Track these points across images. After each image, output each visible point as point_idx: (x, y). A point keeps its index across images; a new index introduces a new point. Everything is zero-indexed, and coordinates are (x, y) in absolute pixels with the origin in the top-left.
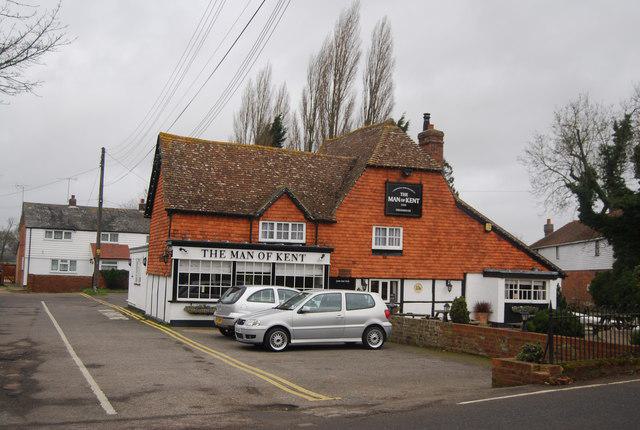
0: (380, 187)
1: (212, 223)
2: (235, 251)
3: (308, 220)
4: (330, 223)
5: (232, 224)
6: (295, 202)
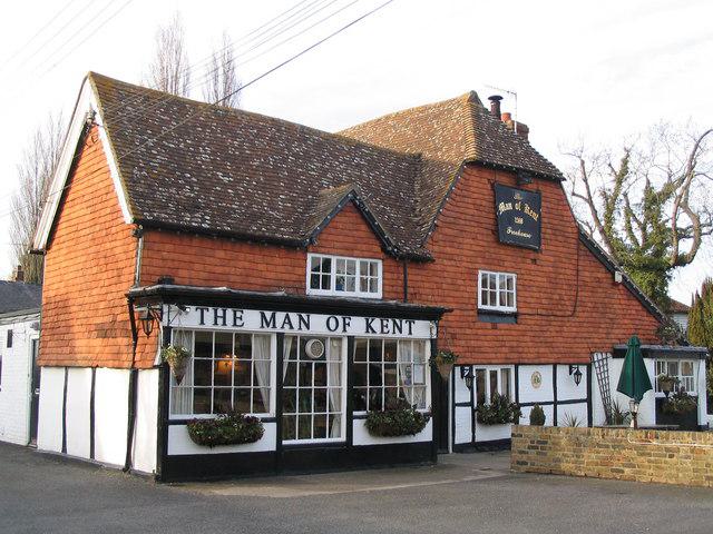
0: (487, 191)
1: (221, 254)
2: (268, 314)
3: (389, 254)
4: (420, 261)
5: (258, 258)
6: (367, 219)
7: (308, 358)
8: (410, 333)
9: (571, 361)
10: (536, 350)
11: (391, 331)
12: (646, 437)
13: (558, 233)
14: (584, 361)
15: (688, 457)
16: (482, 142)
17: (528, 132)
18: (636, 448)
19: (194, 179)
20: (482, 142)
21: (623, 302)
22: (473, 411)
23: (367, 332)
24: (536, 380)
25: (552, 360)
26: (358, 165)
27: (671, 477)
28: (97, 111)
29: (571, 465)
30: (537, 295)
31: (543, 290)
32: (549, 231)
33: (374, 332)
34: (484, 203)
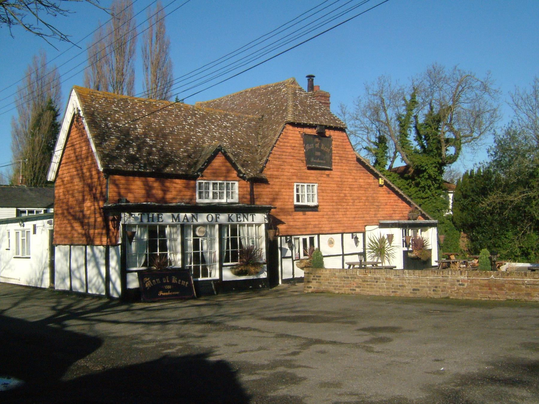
2: (176, 215)
7: (197, 236)
8: (253, 221)
9: (352, 231)
10: (330, 225)
11: (242, 220)
12: (366, 272)
13: (342, 158)
14: (360, 231)
15: (384, 282)
16: (296, 110)
17: (329, 97)
18: (361, 278)
19: (134, 144)
20: (296, 110)
21: (385, 195)
22: (293, 261)
23: (229, 221)
24: (331, 243)
25: (341, 231)
26: (225, 127)
27: (377, 291)
28: (80, 109)
29: (332, 287)
30: (331, 194)
31: (334, 191)
32: (337, 158)
33: (232, 221)
34: (297, 145)
